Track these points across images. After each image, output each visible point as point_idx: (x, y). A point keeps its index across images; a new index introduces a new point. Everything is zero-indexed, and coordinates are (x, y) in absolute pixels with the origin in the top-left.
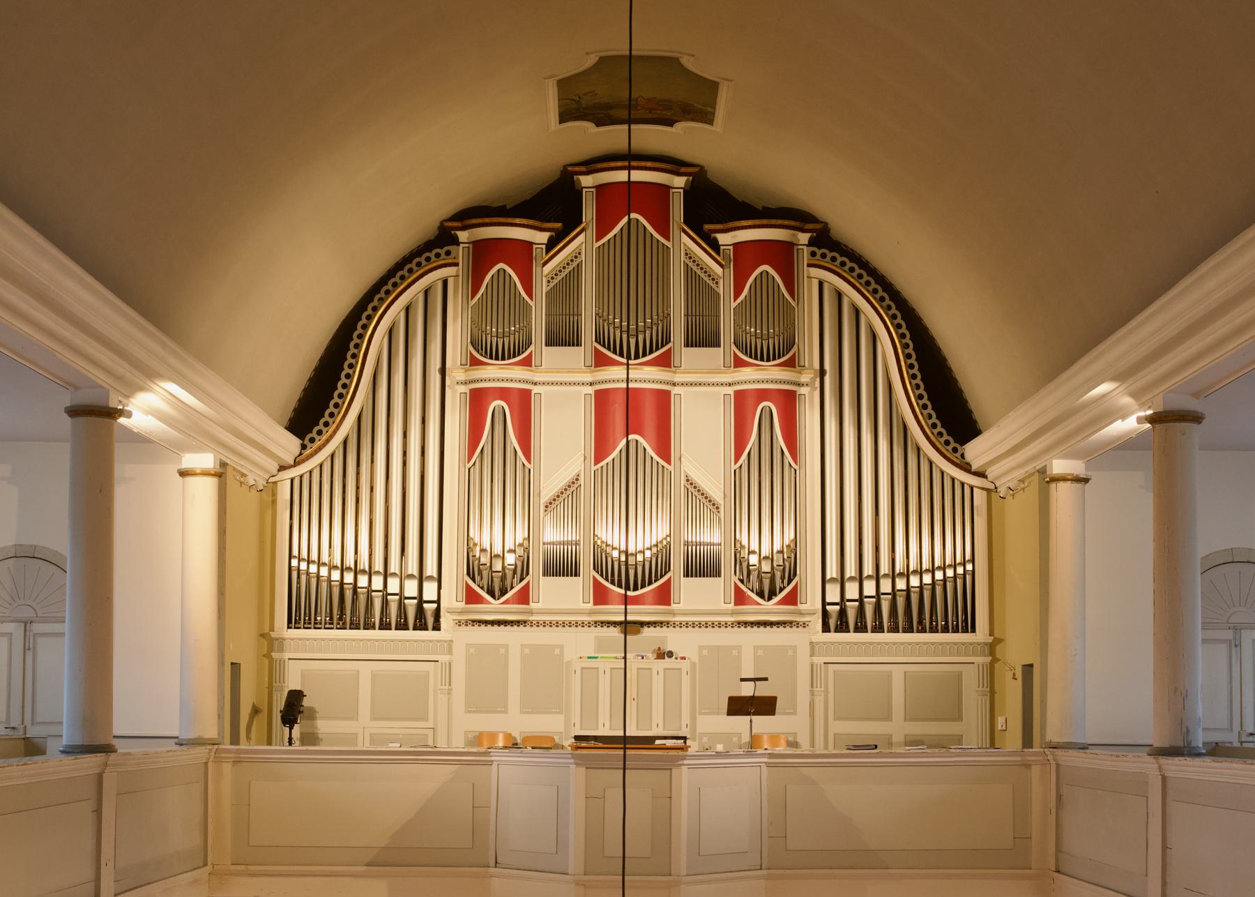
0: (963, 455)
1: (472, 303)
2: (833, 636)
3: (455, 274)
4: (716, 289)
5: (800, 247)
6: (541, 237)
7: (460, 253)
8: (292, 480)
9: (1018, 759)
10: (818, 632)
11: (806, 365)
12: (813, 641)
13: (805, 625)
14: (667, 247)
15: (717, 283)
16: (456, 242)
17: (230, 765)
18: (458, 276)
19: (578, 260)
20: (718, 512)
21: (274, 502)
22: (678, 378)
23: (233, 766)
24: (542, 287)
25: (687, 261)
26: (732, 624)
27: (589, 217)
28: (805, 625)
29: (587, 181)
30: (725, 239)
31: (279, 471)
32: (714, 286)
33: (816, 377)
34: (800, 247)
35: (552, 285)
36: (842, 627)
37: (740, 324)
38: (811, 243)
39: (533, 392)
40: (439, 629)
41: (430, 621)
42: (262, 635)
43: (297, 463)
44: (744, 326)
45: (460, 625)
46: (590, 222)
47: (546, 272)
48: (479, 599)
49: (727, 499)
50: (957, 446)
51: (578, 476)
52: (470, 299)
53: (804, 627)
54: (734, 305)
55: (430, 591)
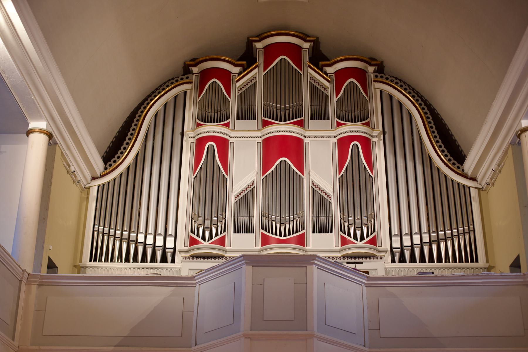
0: (463, 170)
1: (198, 100)
2: (397, 265)
3: (190, 88)
4: (326, 93)
5: (369, 74)
6: (236, 70)
7: (194, 78)
8: (99, 187)
9: (522, 280)
10: (389, 262)
11: (376, 127)
12: (387, 267)
13: (381, 258)
14: (301, 74)
15: (327, 90)
16: (191, 73)
17: (36, 286)
18: (192, 89)
19: (255, 81)
20: (331, 200)
21: (88, 198)
22: (307, 134)
23: (38, 288)
24: (235, 92)
25: (311, 81)
26: (340, 257)
27: (260, 62)
28: (381, 258)
29: (259, 45)
30: (330, 70)
31: (91, 180)
32: (325, 92)
33: (381, 135)
34: (369, 74)
35: (240, 92)
36: (402, 260)
37: (340, 107)
38: (375, 71)
39: (230, 142)
40: (174, 263)
41: (169, 259)
42: (75, 266)
43: (102, 176)
44: (342, 108)
45: (185, 259)
46: (261, 63)
47: (237, 86)
48: (197, 242)
49: (335, 193)
50: (460, 166)
51: (253, 182)
52: (198, 98)
53: (381, 259)
54: (336, 100)
55: (170, 244)
